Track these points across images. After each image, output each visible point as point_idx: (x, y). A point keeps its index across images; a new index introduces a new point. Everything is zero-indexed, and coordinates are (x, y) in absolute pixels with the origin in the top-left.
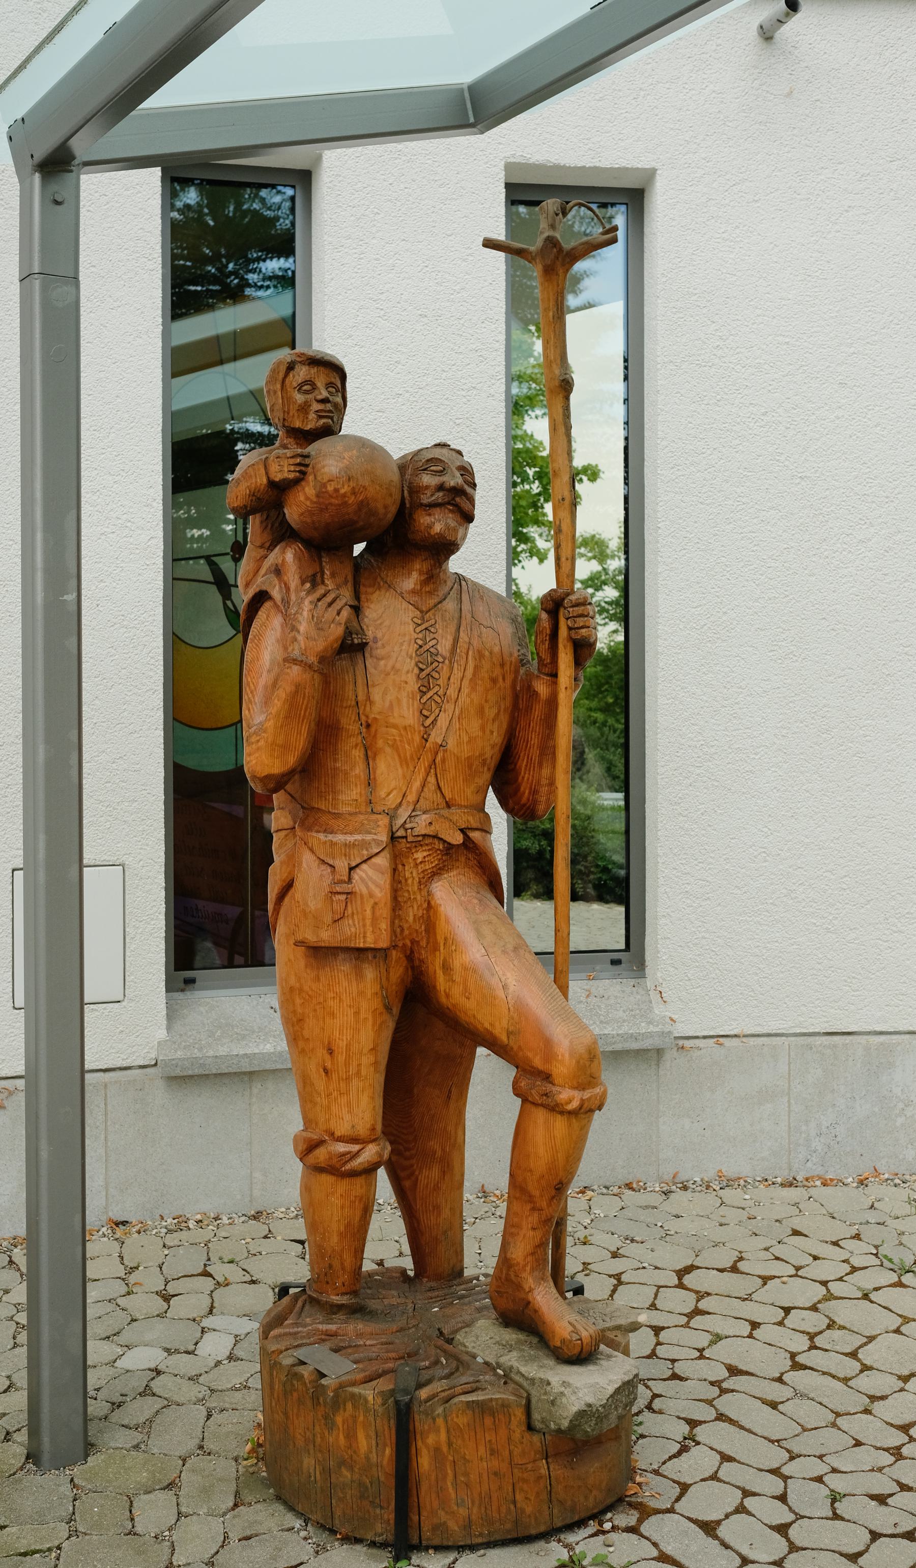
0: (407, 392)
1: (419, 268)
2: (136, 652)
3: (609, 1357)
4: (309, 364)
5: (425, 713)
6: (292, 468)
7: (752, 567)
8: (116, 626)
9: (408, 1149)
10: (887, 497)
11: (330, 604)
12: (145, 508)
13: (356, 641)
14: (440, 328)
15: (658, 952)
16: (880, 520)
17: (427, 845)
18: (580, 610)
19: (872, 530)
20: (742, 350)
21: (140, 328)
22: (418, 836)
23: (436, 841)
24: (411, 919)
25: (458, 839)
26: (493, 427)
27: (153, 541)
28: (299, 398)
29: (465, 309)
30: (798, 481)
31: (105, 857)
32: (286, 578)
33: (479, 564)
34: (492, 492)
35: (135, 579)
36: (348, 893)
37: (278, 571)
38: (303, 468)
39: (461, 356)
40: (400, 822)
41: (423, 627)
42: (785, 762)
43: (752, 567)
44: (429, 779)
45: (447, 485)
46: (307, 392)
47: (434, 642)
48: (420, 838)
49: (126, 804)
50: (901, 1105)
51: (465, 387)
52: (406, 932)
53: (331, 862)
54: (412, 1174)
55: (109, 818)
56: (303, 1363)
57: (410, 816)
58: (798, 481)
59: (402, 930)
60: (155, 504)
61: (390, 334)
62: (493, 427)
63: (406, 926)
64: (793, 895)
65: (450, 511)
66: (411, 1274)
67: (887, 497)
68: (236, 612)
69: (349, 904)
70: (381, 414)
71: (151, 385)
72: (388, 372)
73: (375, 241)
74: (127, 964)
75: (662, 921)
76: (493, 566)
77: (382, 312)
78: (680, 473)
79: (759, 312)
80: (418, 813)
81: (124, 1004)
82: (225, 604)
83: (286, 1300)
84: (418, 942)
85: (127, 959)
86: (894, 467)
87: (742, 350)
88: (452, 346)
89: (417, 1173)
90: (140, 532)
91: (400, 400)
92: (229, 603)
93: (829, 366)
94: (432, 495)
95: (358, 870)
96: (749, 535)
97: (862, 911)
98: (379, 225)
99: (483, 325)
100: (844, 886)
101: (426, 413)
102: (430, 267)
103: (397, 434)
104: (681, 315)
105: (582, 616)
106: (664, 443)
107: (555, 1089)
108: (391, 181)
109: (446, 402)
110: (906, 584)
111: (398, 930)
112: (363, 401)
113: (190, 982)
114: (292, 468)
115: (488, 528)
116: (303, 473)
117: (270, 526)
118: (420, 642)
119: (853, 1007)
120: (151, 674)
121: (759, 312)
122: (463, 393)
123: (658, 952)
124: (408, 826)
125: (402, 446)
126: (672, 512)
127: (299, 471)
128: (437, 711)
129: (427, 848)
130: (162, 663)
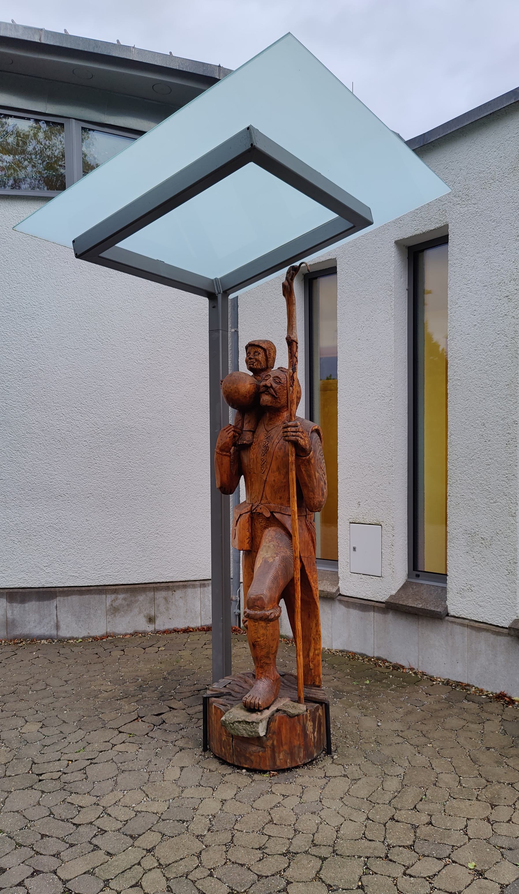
11: (227, 431)
25: (268, 515)
109: (494, 324)
122: (501, 318)
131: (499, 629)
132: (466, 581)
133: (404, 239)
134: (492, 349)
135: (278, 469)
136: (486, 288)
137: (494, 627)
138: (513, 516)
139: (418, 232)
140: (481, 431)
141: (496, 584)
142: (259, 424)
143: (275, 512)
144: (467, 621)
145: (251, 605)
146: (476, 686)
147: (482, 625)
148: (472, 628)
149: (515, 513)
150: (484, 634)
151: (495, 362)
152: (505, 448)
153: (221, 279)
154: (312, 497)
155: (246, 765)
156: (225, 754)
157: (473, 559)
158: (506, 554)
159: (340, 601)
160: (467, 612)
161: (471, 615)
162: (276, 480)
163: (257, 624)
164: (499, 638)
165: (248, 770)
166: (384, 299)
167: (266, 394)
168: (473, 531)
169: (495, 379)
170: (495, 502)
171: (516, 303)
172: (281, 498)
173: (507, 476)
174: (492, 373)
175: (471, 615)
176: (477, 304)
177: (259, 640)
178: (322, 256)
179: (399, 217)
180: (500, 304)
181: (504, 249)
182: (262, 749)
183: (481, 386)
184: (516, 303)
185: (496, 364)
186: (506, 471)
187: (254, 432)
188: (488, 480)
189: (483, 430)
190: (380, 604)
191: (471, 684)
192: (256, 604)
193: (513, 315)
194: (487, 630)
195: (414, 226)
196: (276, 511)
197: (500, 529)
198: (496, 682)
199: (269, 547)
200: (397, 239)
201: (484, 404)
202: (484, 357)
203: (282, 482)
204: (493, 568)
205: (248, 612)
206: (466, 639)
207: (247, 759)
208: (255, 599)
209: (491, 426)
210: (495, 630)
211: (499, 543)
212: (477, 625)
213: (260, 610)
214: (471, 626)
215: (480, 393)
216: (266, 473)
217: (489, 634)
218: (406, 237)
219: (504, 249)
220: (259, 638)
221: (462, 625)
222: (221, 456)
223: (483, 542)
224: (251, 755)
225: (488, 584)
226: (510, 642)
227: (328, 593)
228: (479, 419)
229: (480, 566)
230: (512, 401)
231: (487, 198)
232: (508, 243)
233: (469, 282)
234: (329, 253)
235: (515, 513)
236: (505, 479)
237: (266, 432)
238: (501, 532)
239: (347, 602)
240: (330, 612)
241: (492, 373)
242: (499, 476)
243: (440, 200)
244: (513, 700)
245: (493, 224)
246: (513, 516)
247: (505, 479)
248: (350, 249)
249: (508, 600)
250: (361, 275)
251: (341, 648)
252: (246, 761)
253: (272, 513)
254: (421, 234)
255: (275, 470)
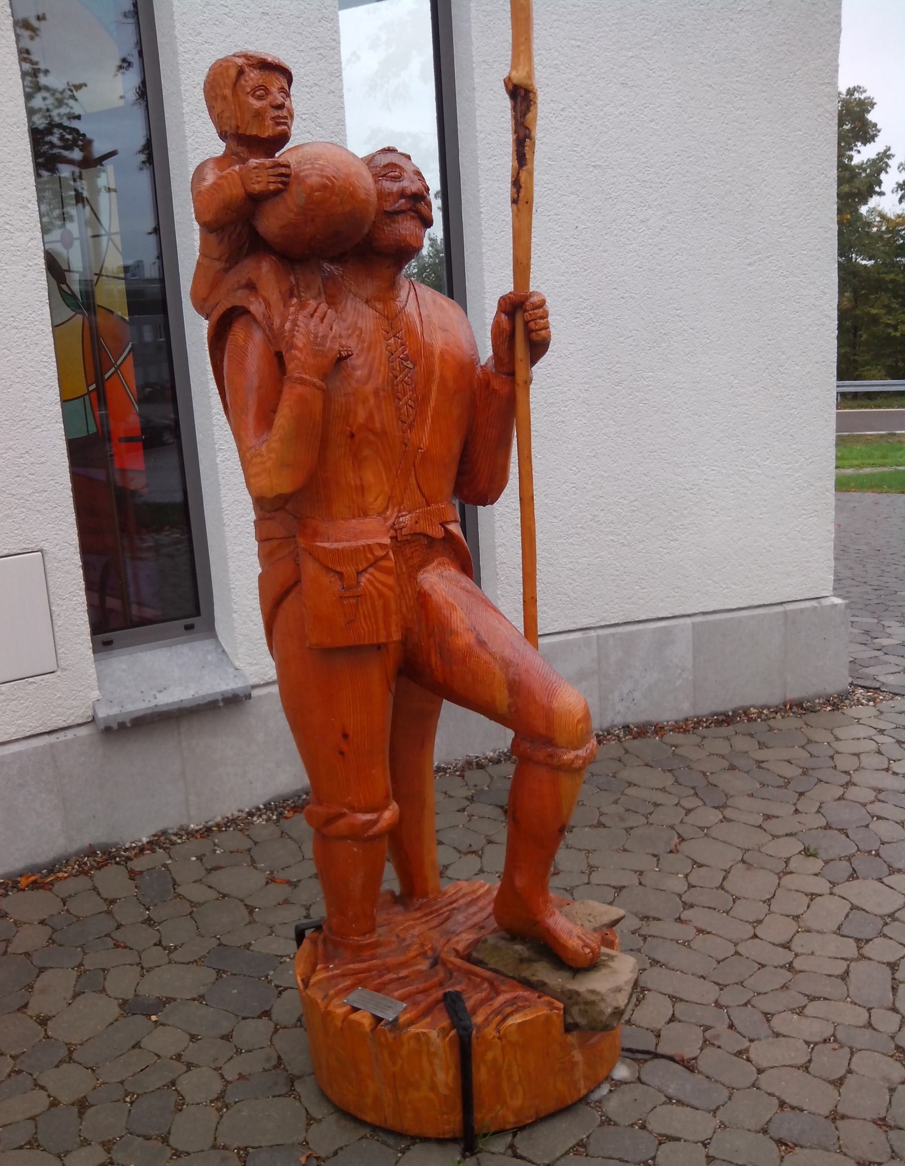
2: (29, 351)
3: (612, 958)
4: (260, 68)
6: (272, 179)
7: (558, 246)
8: (7, 328)
10: (661, 183)
12: (21, 210)
14: (281, 26)
15: (497, 574)
16: (656, 203)
19: (650, 211)
20: (543, 52)
23: (422, 537)
26: (335, 121)
27: (34, 242)
28: (256, 104)
29: (302, 8)
30: (591, 169)
31: (24, 546)
32: (264, 293)
35: (20, 281)
36: (358, 596)
37: (251, 287)
38: (284, 179)
39: (303, 54)
42: (588, 412)
43: (558, 246)
45: (408, 192)
46: (260, 98)
49: (37, 495)
50: (679, 671)
51: (307, 84)
53: (338, 569)
55: (23, 510)
56: (355, 1010)
58: (591, 169)
60: (30, 205)
61: (236, 31)
62: (335, 121)
64: (596, 519)
65: (412, 218)
66: (397, 893)
67: (661, 183)
68: (73, 295)
69: (360, 607)
71: (10, 82)
74: (57, 639)
75: (499, 550)
77: (227, 10)
78: (496, 163)
79: (555, 17)
80: (404, 513)
81: (58, 673)
82: (60, 289)
83: (306, 943)
85: (56, 634)
86: (665, 157)
87: (543, 52)
88: (294, 44)
90: (19, 234)
92: (64, 286)
93: (612, 68)
94: (395, 202)
96: (555, 217)
97: (648, 526)
100: (634, 508)
104: (491, 18)
106: (482, 136)
107: (559, 751)
110: (677, 257)
113: (108, 644)
114: (272, 179)
117: (226, 238)
119: (642, 601)
120: (45, 370)
121: (555, 17)
123: (497, 574)
124: (396, 527)
126: (492, 198)
127: (280, 182)
130: (55, 360)
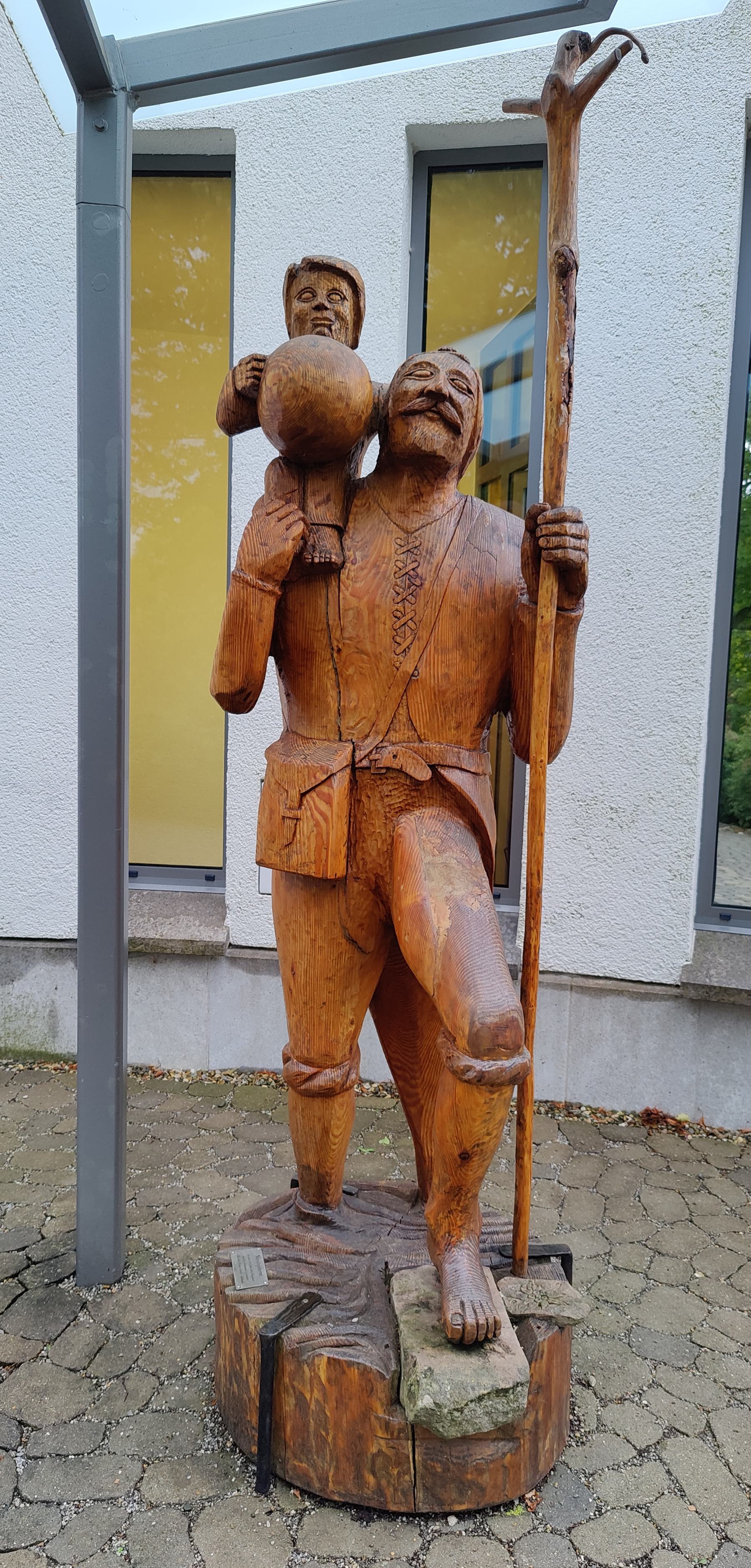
0: (627, 354)
1: (647, 225)
5: (398, 639)
9: (414, 1078)
11: (280, 520)
13: (317, 560)
17: (392, 778)
18: (556, 528)
21: (380, 309)
22: (382, 768)
24: (374, 853)
25: (424, 774)
33: (688, 525)
34: (707, 452)
38: (257, 373)
40: (363, 753)
41: (405, 549)
44: (401, 711)
46: (306, 300)
47: (415, 565)
48: (383, 771)
52: (369, 866)
54: (418, 1101)
57: (377, 747)
59: (365, 864)
63: (368, 859)
70: (599, 378)
72: (609, 335)
73: (603, 202)
76: (703, 527)
77: (607, 275)
84: (382, 877)
89: (422, 1102)
91: (619, 363)
95: (307, 796)
98: (608, 184)
99: (711, 278)
101: (644, 375)
102: (658, 222)
103: (613, 397)
105: (557, 534)
108: (623, 137)
109: (666, 362)
111: (361, 863)
112: (583, 366)
115: (700, 489)
116: (258, 378)
118: (400, 565)
122: (684, 351)
125: (619, 409)
128: (411, 638)
129: (392, 781)
131: (644, 986)
132: (569, 897)
133: (432, 126)
134: (658, 414)
135: (461, 642)
136: (650, 278)
137: (630, 984)
138: (691, 764)
139: (472, 117)
140: (621, 587)
141: (640, 901)
142: (354, 510)
143: (444, 766)
144: (565, 977)
145: (486, 1044)
146: (585, 1104)
147: (601, 982)
148: (583, 990)
149: (695, 758)
150: (609, 1002)
151: (665, 443)
152: (679, 624)
153: (126, 43)
154: (559, 723)
155: (461, 1503)
156: (380, 1491)
157: (588, 852)
158: (670, 838)
159: (233, 960)
160: (566, 959)
161: (575, 966)
162: (452, 673)
163: (495, 1096)
164: (646, 1005)
165: (461, 1516)
166: (375, 259)
167: (431, 419)
168: (590, 794)
169: (662, 480)
170: (647, 736)
171: (722, 323)
172: (458, 726)
173: (680, 682)
174: (656, 466)
175: (575, 966)
176: (626, 312)
177: (487, 1138)
178: (190, 116)
179: (421, 68)
180: (682, 320)
181: (700, 201)
182: (511, 1444)
183: (626, 492)
184: (722, 323)
185: (666, 447)
186: (680, 673)
187: (341, 531)
188: (633, 689)
189: (626, 585)
190: (553, 977)
191: (574, 1101)
192: (501, 1040)
193: (714, 348)
194: (619, 993)
195: (463, 99)
196: (449, 762)
197: (658, 789)
198: (635, 1091)
199: (446, 865)
200: (413, 121)
201: (632, 532)
202: (636, 429)
203: (470, 681)
204: (637, 868)
205: (478, 1068)
206: (567, 1014)
207: (463, 1487)
208: (498, 1026)
209: (646, 578)
210: (641, 990)
211: (653, 817)
212: (591, 983)
213: (509, 1056)
214: (581, 987)
215: (623, 507)
216: (414, 652)
217: (624, 999)
218: (438, 121)
219: (700, 201)
220: (488, 1134)
221: (561, 987)
222: (260, 595)
223: (614, 816)
224: (480, 1471)
225: (621, 901)
226: (673, 1011)
227: (207, 945)
228: (617, 561)
229: (603, 865)
230: (700, 529)
231: (662, 79)
232: (710, 191)
233: (607, 259)
234: (213, 114)
235: (695, 758)
236: (677, 689)
237: (403, 535)
238: (659, 796)
239: (253, 960)
240: (202, 986)
241: (656, 466)
242: (659, 682)
243: (699, 22)
244: (680, 1122)
245: (675, 139)
246: (691, 764)
247: (677, 689)
248: (279, 115)
249: (669, 930)
250: (309, 188)
251: (235, 1065)
252: (461, 1493)
253: (433, 767)
254: (478, 123)
255: (450, 644)
